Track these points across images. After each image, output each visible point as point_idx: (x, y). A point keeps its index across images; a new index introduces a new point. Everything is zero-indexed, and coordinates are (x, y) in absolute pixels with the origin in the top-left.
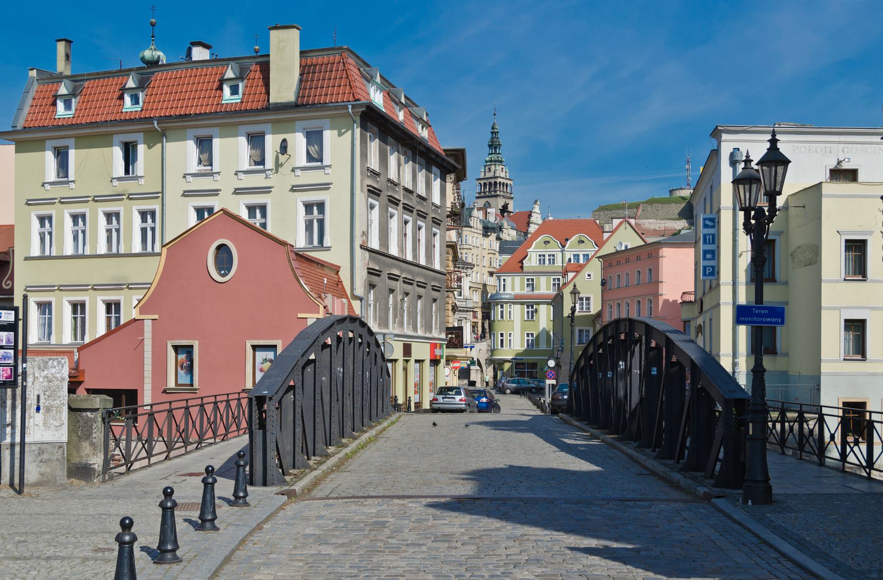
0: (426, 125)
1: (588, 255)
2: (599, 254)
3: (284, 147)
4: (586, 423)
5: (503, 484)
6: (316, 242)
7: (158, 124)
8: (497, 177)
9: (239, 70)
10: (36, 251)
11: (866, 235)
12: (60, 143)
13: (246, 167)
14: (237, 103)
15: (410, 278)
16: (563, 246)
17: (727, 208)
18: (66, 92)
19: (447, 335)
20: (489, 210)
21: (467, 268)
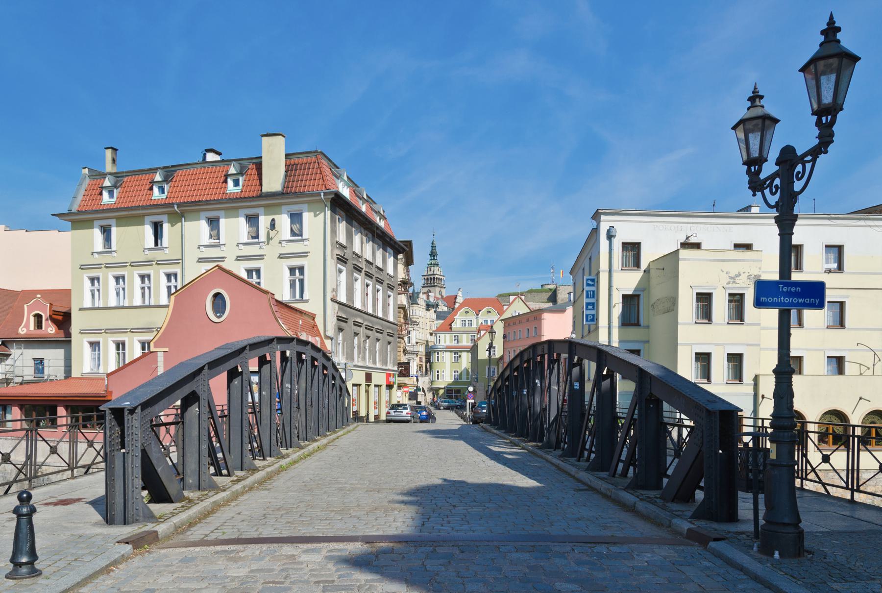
0: (383, 217)
1: (493, 321)
2: (501, 319)
3: (273, 225)
4: (503, 431)
5: (434, 511)
6: (298, 296)
7: (177, 208)
8: (435, 274)
9: (239, 169)
10: (88, 304)
11: (712, 289)
12: (105, 223)
13: (245, 240)
14: (237, 193)
15: (371, 325)
16: (478, 315)
17: (604, 271)
18: (110, 185)
19: (398, 368)
20: (430, 294)
21: (414, 324)
